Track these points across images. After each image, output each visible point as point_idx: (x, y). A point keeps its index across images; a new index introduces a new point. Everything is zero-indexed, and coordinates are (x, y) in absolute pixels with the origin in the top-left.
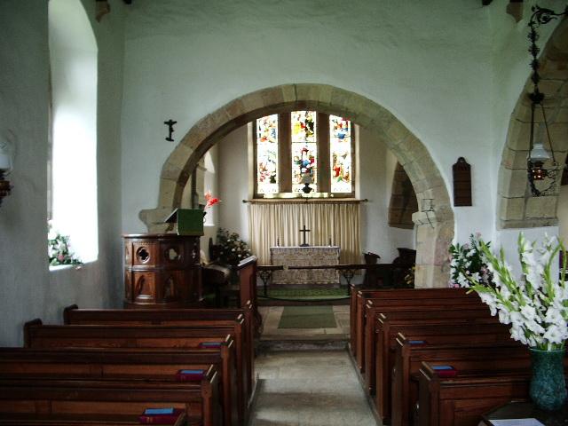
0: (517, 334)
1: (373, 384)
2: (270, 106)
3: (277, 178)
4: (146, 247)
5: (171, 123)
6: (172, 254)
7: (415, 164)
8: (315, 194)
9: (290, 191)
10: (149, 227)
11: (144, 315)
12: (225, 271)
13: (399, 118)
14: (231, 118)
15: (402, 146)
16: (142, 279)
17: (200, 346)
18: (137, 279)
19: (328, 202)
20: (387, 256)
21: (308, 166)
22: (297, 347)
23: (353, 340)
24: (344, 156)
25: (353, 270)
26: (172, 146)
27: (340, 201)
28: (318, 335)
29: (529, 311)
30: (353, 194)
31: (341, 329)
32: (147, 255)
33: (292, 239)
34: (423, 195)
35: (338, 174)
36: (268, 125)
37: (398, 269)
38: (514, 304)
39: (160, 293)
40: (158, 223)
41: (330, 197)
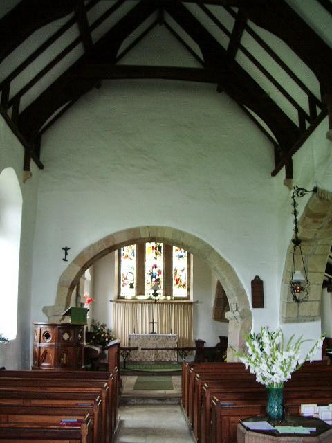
0: (259, 379)
1: (193, 421)
2: (131, 240)
3: (134, 285)
4: (49, 331)
5: (66, 249)
6: (66, 336)
7: (227, 280)
8: (161, 297)
9: (144, 294)
10: (49, 318)
11: (47, 374)
12: (98, 349)
13: (217, 250)
14: (106, 247)
15: (218, 268)
16: (46, 352)
17: (77, 404)
18: (42, 352)
19: (171, 303)
20: (211, 342)
21: (157, 277)
22: (146, 402)
23: (183, 397)
24: (183, 271)
25: (187, 351)
26: (66, 264)
27: (178, 302)
28: (160, 394)
29: (264, 366)
30: (188, 298)
31: (176, 391)
32: (50, 336)
33: (144, 329)
34: (232, 301)
35: (177, 283)
36: (129, 251)
37: (219, 351)
38: (257, 363)
39: (58, 361)
40: (55, 316)
41: (172, 299)
